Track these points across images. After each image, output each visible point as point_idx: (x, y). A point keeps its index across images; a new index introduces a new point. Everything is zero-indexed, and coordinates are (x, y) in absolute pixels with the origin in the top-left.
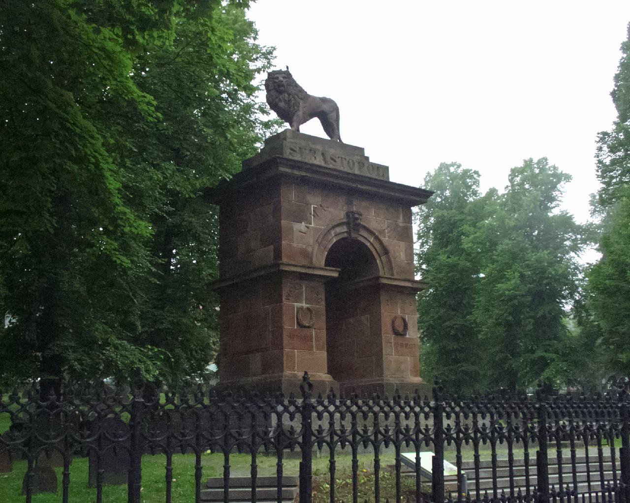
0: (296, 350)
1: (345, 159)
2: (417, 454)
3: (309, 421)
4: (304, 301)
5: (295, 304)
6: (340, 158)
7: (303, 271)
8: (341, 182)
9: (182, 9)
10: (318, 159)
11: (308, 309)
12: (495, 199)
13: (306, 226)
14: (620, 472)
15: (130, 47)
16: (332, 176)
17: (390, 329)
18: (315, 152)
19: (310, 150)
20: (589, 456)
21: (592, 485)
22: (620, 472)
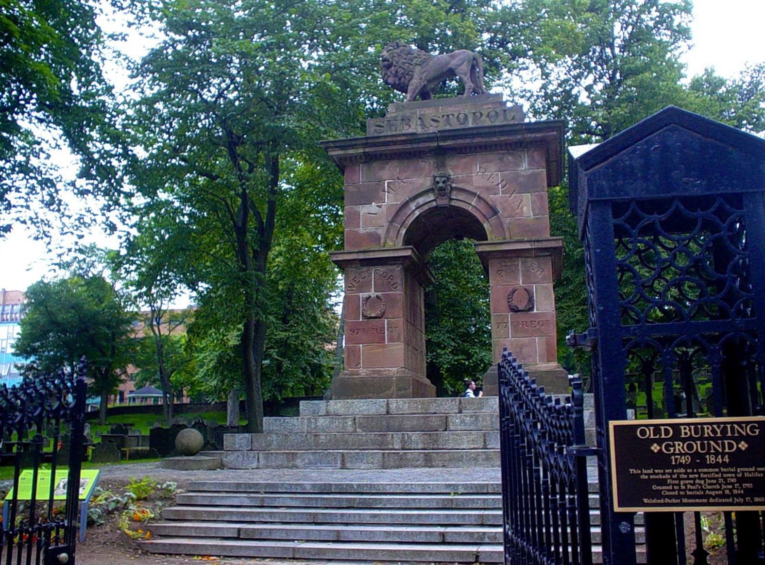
0: (361, 345)
1: (453, 115)
2: (70, 475)
3: (725, 411)
4: (373, 289)
5: (361, 294)
6: (445, 117)
7: (362, 256)
8: (409, 146)
9: (88, 36)
10: (413, 126)
11: (378, 297)
12: (224, 81)
13: (378, 206)
14: (598, 512)
15: (190, 96)
16: (395, 143)
17: (504, 304)
18: (409, 120)
19: (403, 120)
20: (55, 498)
21: (593, 533)
22: (598, 512)
